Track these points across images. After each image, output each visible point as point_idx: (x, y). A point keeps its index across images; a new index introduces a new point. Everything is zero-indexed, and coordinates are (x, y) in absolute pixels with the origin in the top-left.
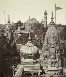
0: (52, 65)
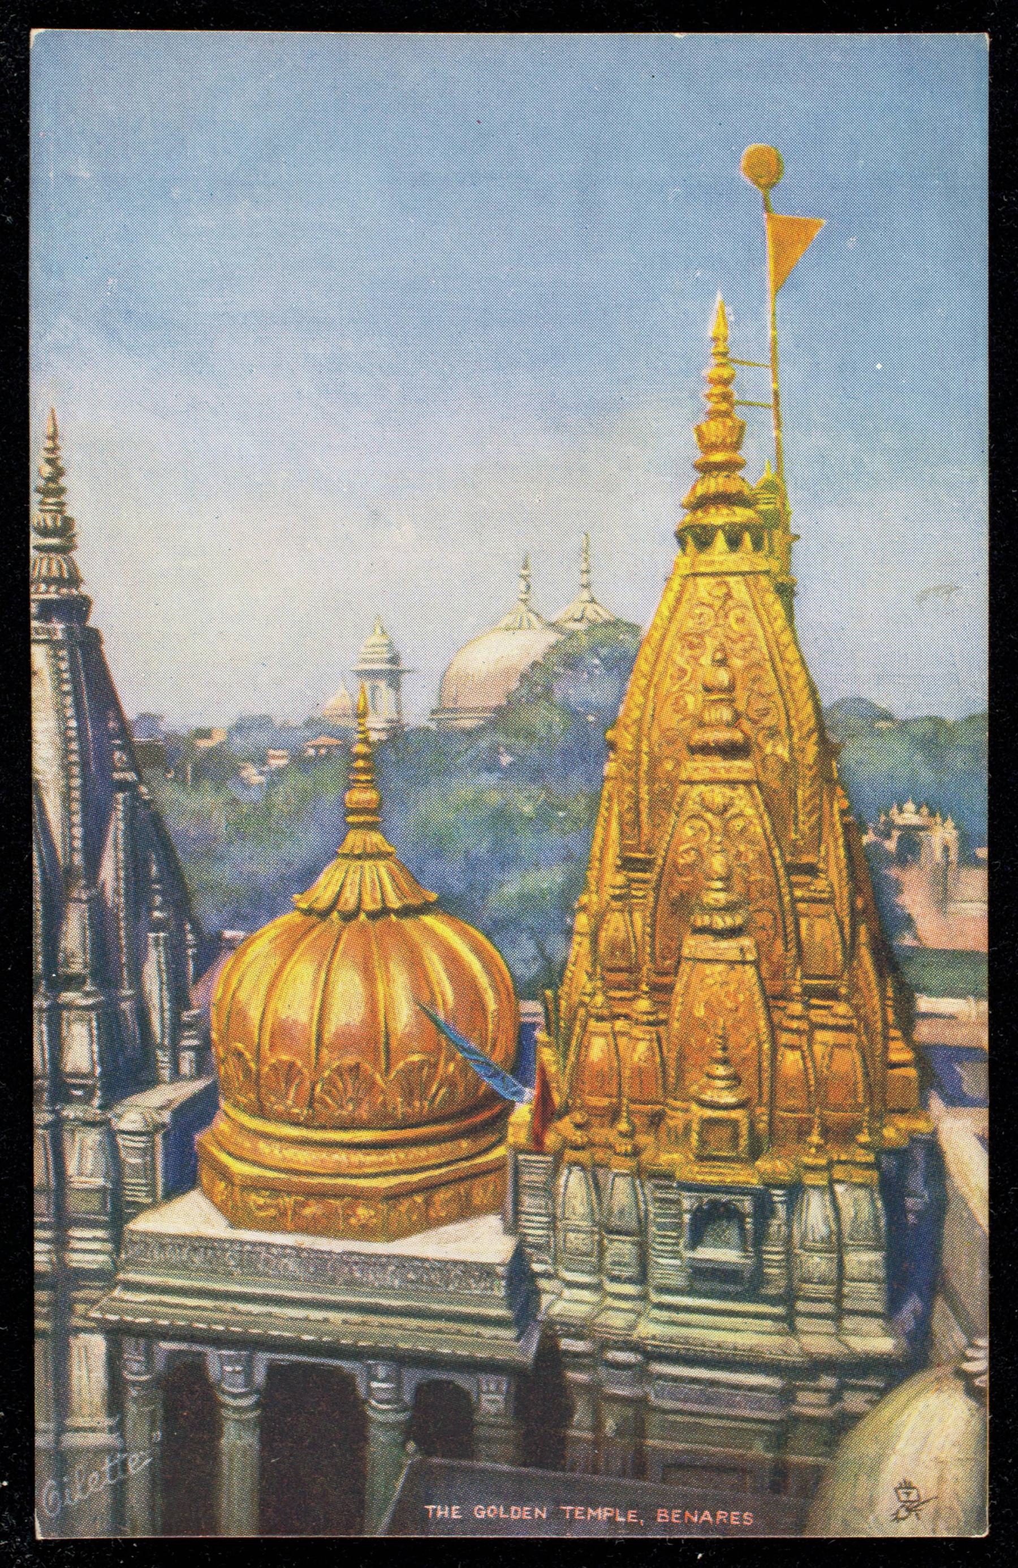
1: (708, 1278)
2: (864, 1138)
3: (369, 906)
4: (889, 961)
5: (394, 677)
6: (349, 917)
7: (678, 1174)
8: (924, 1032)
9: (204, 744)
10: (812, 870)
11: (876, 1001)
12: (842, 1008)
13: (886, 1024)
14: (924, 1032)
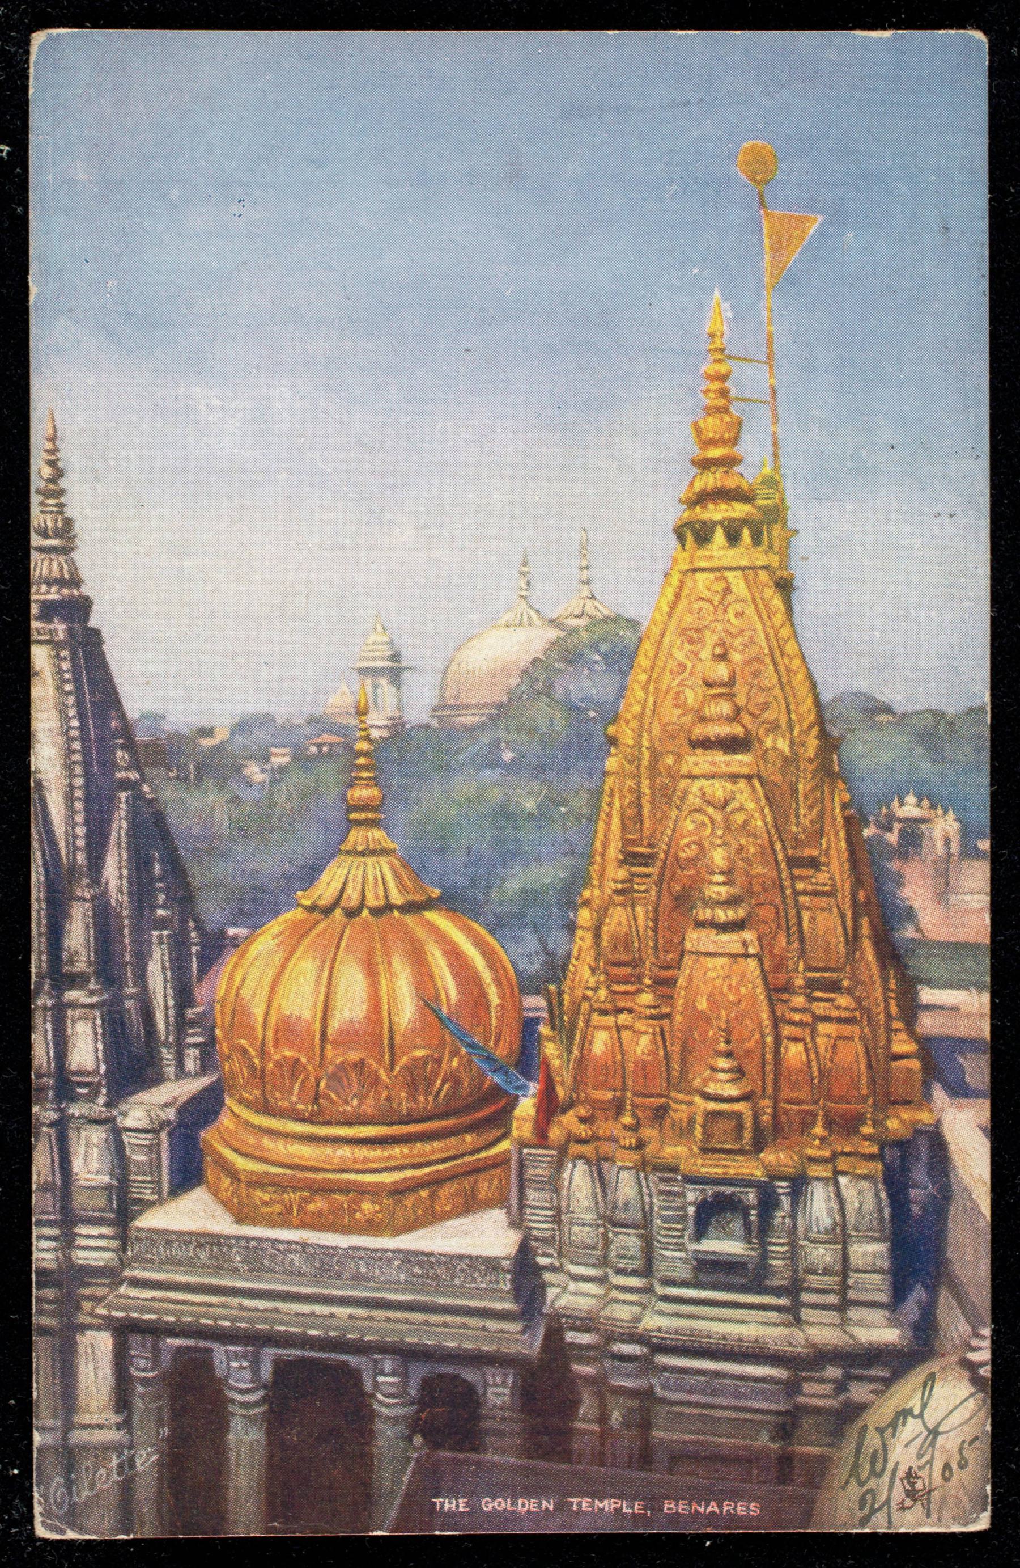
0: (716, 1245)
1: (713, 1271)
2: (867, 1130)
3: (372, 902)
4: (892, 955)
5: (395, 673)
6: (351, 913)
7: (682, 1167)
8: (928, 1024)
9: (206, 742)
10: (814, 863)
11: (879, 992)
12: (843, 1000)
13: (889, 1016)
14: (928, 1024)
